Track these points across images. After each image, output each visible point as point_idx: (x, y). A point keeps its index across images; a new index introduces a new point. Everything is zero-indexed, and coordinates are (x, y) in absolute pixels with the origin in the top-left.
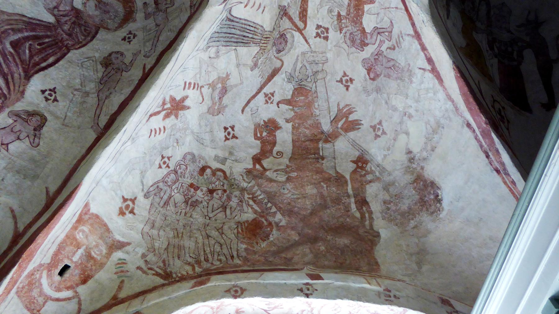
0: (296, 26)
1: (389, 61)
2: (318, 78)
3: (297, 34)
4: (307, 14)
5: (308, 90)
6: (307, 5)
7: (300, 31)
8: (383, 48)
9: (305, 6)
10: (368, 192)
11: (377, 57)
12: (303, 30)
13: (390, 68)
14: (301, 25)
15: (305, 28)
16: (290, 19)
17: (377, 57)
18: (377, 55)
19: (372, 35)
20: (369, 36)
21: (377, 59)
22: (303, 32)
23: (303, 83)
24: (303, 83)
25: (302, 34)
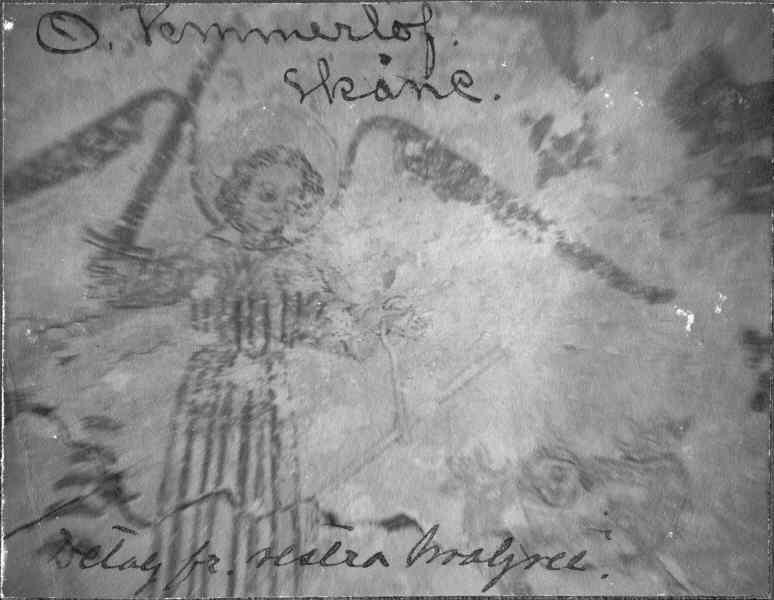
0: (171, 140)
7: (184, 112)
12: (172, 95)
14: (160, 114)
15: (156, 95)
16: (136, 211)
25: (196, 87)
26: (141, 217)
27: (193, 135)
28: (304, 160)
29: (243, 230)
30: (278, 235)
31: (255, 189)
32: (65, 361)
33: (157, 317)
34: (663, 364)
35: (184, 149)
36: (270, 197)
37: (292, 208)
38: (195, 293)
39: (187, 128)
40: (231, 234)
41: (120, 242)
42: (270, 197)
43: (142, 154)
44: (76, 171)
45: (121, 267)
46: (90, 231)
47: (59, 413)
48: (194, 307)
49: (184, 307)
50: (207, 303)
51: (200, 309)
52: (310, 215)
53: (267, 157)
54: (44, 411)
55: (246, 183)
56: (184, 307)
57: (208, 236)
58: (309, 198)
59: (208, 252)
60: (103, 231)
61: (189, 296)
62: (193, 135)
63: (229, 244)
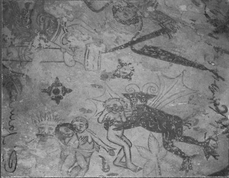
0: (139, 40)
1: (85, 158)
2: (66, 54)
3: (129, 38)
4: (152, 56)
5: (52, 37)
6: (164, 59)
7: (132, 43)
8: (103, 152)
9: (162, 57)
10: (218, 171)
11: (90, 140)
12: (132, 47)
13: (76, 161)
14: (137, 47)
15: (135, 51)
16: (157, 34)
17: (90, 140)
18: (93, 140)
19: (122, 137)
20: (120, 133)
21: (87, 141)
22: (129, 49)
23: (62, 31)
24: (62, 31)
25: (126, 45)
26: (157, 32)
27: (134, 38)
28: (114, 15)
29: (136, 12)
30: (128, 6)
31: (128, 18)
32: (194, 21)
33: (165, 11)
34: (194, 14)
35: (138, 37)
36: (126, 14)
37: (122, 9)
38: (154, 10)
39: (135, 39)
40: (139, 14)
41: (164, 31)
42: (126, 14)
43: (148, 43)
44: (163, 51)
45: (168, 26)
46: (170, 38)
47: (204, 13)
48: (156, 7)
49: (158, 9)
50: (152, 6)
51: (154, 6)
52: (119, 4)
53: (121, 21)
54: (206, 15)
55: (129, 20)
56: (158, 9)
57: (144, 17)
58: (117, 7)
59: (147, 15)
60: (167, 35)
61: (155, 10)
62: (134, 38)
63: (141, 12)
